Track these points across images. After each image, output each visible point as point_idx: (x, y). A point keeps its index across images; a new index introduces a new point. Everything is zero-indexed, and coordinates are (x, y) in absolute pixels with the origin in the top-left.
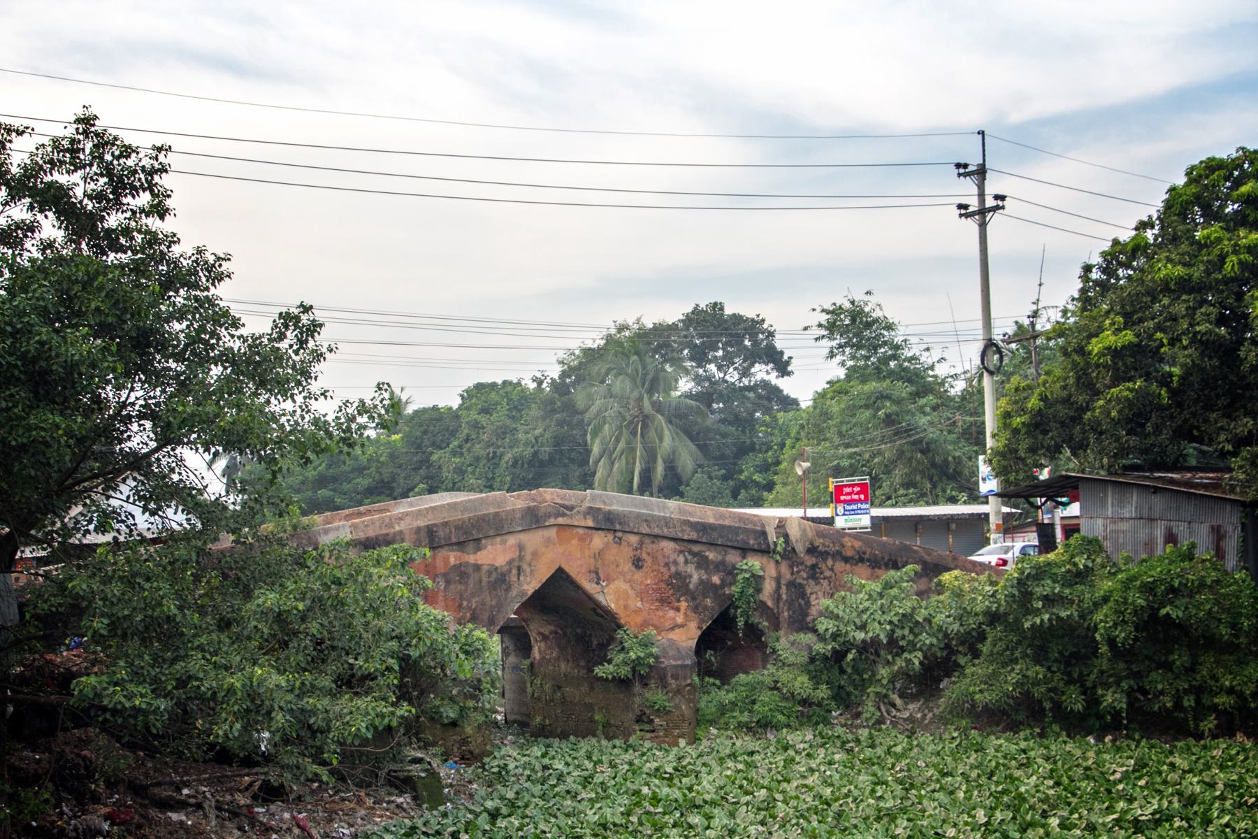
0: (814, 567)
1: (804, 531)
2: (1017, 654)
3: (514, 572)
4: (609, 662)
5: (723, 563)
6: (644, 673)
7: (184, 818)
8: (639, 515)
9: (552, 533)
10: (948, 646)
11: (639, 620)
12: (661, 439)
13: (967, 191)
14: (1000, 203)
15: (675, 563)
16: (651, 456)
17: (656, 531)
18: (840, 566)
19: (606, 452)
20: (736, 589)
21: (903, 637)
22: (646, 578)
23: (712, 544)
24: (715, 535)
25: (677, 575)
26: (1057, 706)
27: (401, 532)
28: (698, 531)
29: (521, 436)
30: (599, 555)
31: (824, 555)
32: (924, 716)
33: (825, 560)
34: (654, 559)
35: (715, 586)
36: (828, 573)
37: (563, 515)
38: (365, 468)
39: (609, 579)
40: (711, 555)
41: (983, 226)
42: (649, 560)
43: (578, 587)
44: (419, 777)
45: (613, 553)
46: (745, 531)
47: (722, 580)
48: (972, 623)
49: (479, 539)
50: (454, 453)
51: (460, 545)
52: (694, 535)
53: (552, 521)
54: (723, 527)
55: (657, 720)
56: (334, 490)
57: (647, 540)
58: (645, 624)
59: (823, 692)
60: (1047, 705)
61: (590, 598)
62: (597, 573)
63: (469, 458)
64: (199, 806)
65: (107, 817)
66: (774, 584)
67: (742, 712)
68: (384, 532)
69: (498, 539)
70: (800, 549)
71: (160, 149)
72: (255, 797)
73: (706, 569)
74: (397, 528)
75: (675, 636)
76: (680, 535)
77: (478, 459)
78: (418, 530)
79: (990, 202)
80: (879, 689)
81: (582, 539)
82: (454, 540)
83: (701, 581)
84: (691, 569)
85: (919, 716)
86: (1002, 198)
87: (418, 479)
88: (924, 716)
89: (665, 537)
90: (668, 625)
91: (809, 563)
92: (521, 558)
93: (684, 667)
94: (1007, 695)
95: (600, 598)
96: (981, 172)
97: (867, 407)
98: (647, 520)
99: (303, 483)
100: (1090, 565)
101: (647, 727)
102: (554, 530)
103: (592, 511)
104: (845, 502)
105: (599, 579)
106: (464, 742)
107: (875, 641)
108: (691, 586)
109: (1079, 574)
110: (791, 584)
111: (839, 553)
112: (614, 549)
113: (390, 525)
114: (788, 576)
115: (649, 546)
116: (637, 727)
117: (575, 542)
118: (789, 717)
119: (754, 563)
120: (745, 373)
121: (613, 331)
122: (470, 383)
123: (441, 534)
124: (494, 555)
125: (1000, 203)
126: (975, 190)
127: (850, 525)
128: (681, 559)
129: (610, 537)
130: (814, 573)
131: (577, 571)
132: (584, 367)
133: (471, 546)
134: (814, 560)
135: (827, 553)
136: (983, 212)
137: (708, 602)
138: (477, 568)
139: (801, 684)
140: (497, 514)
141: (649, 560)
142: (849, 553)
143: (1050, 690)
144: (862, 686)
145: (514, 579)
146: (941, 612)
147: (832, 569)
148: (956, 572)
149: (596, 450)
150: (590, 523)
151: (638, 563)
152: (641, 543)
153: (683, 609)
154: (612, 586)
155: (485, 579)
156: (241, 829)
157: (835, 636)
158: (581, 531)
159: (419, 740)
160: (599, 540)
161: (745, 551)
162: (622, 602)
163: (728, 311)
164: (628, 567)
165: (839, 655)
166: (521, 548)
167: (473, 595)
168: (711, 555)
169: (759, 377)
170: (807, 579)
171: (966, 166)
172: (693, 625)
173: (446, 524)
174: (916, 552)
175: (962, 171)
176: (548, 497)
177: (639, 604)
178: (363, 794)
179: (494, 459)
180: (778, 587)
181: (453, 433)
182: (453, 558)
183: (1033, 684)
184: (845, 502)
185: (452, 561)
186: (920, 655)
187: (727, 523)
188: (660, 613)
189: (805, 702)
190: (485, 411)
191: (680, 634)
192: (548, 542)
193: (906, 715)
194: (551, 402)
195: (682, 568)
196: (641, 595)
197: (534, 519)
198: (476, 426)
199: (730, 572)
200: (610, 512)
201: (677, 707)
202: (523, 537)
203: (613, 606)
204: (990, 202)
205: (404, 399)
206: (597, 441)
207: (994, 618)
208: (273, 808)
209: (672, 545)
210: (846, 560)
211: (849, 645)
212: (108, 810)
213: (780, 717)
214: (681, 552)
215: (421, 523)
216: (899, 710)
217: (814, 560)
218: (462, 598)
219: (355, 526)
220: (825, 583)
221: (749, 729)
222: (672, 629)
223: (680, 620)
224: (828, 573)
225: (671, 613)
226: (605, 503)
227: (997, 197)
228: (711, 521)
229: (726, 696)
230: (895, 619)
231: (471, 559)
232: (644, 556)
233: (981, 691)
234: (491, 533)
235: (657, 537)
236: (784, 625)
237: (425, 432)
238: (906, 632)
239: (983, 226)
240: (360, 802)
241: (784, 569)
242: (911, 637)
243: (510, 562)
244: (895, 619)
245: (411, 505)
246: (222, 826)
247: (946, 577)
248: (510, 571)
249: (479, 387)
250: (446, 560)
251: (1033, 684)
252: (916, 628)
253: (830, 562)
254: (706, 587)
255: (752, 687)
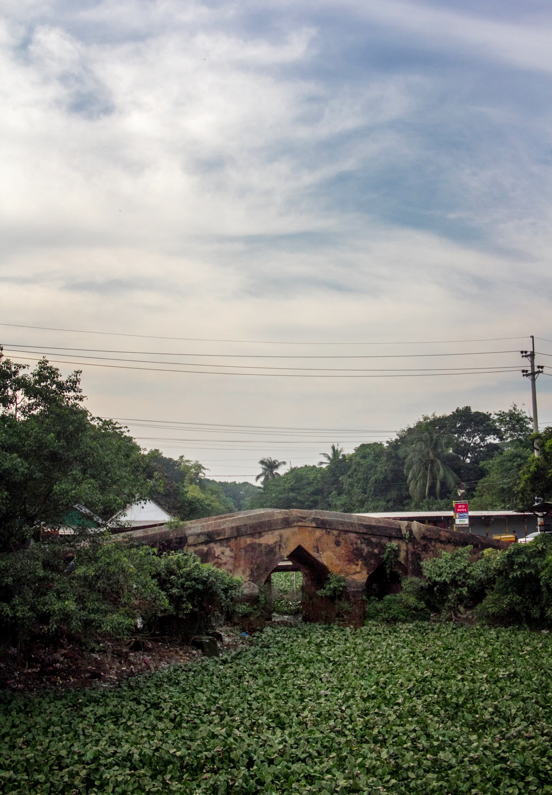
0: (425, 546)
1: (420, 529)
2: (510, 590)
3: (278, 547)
4: (324, 588)
5: (379, 543)
6: (340, 594)
7: (97, 656)
8: (338, 521)
9: (296, 529)
10: (482, 585)
11: (338, 569)
12: (439, 471)
13: (526, 363)
14: (541, 370)
15: (356, 543)
16: (434, 478)
17: (346, 528)
18: (438, 545)
19: (414, 477)
20: (385, 556)
21: (460, 580)
22: (341, 550)
23: (374, 535)
24: (375, 530)
25: (357, 549)
26: (528, 615)
27: (224, 529)
28: (367, 529)
29: (379, 469)
30: (318, 540)
31: (430, 540)
32: (473, 617)
33: (431, 542)
34: (346, 542)
35: (375, 554)
36: (432, 548)
37: (301, 521)
38: (312, 483)
39: (323, 551)
40: (374, 540)
41: (533, 380)
42: (343, 542)
43: (309, 554)
44: (206, 642)
45: (326, 538)
46: (391, 529)
47: (379, 552)
48: (491, 575)
49: (261, 533)
50: (349, 477)
51: (252, 535)
52: (365, 531)
53: (296, 524)
54: (379, 527)
55: (345, 616)
56: (298, 493)
57: (342, 533)
58: (341, 571)
59: (422, 605)
60: (523, 614)
61: (314, 558)
62: (317, 548)
63: (355, 478)
64: (105, 652)
65: (63, 655)
66: (405, 554)
67: (385, 613)
68: (216, 529)
69: (270, 532)
70: (417, 537)
71: (77, 372)
72: (131, 649)
73: (372, 547)
74: (222, 527)
75: (355, 577)
76: (358, 530)
77: (360, 479)
78: (232, 528)
79: (536, 370)
80: (449, 604)
81: (310, 532)
82: (249, 533)
83: (369, 552)
84: (363, 546)
85: (470, 617)
86: (542, 367)
87: (333, 488)
88: (473, 617)
89: (351, 532)
90: (352, 571)
91: (422, 544)
92: (281, 541)
93: (358, 592)
94: (503, 609)
95: (319, 559)
96: (532, 355)
97: (509, 460)
98: (342, 524)
99: (284, 489)
100: (545, 548)
101: (341, 619)
102: (297, 528)
103: (314, 520)
104: (459, 512)
105: (318, 550)
106: (250, 624)
107: (445, 582)
108: (364, 554)
109: (539, 552)
110: (413, 554)
111: (438, 539)
112: (326, 537)
113: (220, 526)
114: (412, 550)
115: (343, 536)
116: (337, 619)
117: (307, 534)
118: (406, 616)
119: (394, 544)
120: (482, 440)
121: (422, 420)
122: (358, 445)
123: (243, 530)
124: (268, 539)
125: (541, 370)
126: (530, 364)
127: (461, 523)
128: (359, 542)
129: (324, 531)
130: (425, 548)
131: (308, 546)
132: (408, 437)
133: (257, 535)
134: (425, 542)
135: (432, 539)
136: (533, 374)
137: (372, 561)
138: (260, 545)
139: (412, 600)
140: (269, 521)
141: (343, 542)
142: (443, 539)
143: (524, 607)
144: (442, 602)
145: (277, 550)
146: (477, 570)
147: (434, 546)
148: (490, 549)
149: (410, 476)
150: (314, 525)
151: (337, 543)
152: (339, 534)
153: (360, 565)
154: (325, 554)
155: (264, 550)
156: (120, 662)
157: (430, 579)
158: (310, 529)
159: (231, 622)
160: (318, 533)
161: (390, 538)
162: (329, 561)
163: (473, 410)
164: (333, 545)
165: (431, 588)
166: (281, 536)
167: (258, 557)
168: (374, 540)
169: (488, 442)
170: (422, 551)
171: (526, 352)
172: (365, 572)
173: (245, 525)
174: (477, 538)
175: (524, 354)
176: (294, 513)
177: (338, 562)
178: (178, 649)
179: (367, 480)
180: (407, 555)
181: (350, 467)
182: (249, 540)
183: (516, 604)
184: (459, 512)
185: (248, 542)
186: (466, 588)
187: (381, 525)
188: (348, 566)
189: (416, 609)
190: (364, 457)
191: (359, 575)
192: (294, 533)
193: (465, 616)
194: (390, 454)
195: (359, 546)
196: (338, 558)
197: (287, 523)
198: (359, 464)
199: (383, 548)
200: (323, 520)
201: (354, 610)
202: (282, 531)
203: (325, 563)
204: (536, 370)
205: (339, 450)
206: (411, 472)
207: (500, 572)
208: (137, 653)
209: (354, 535)
210: (441, 542)
211: (435, 583)
212: (66, 651)
213: (401, 616)
214: (359, 538)
215: (234, 525)
216: (461, 614)
217: (425, 542)
218: (252, 558)
219: (203, 526)
220: (431, 553)
221: (388, 622)
222: (355, 574)
223: (358, 569)
224: (432, 548)
225: (354, 567)
226: (321, 516)
227: (539, 367)
228: (374, 524)
229: (380, 606)
230: (456, 572)
231: (257, 541)
232: (341, 540)
233: (492, 607)
234: (266, 529)
235: (346, 532)
236: (410, 572)
237: (337, 467)
238: (461, 578)
239: (533, 380)
240: (177, 652)
241: (410, 546)
242: (464, 580)
243: (276, 543)
244: (456, 572)
245: (245, 514)
246: (113, 661)
247: (485, 551)
248: (275, 547)
249: (363, 446)
250: (246, 542)
251: (516, 604)
252: (467, 576)
253: (433, 543)
254: (371, 555)
255: (390, 601)
